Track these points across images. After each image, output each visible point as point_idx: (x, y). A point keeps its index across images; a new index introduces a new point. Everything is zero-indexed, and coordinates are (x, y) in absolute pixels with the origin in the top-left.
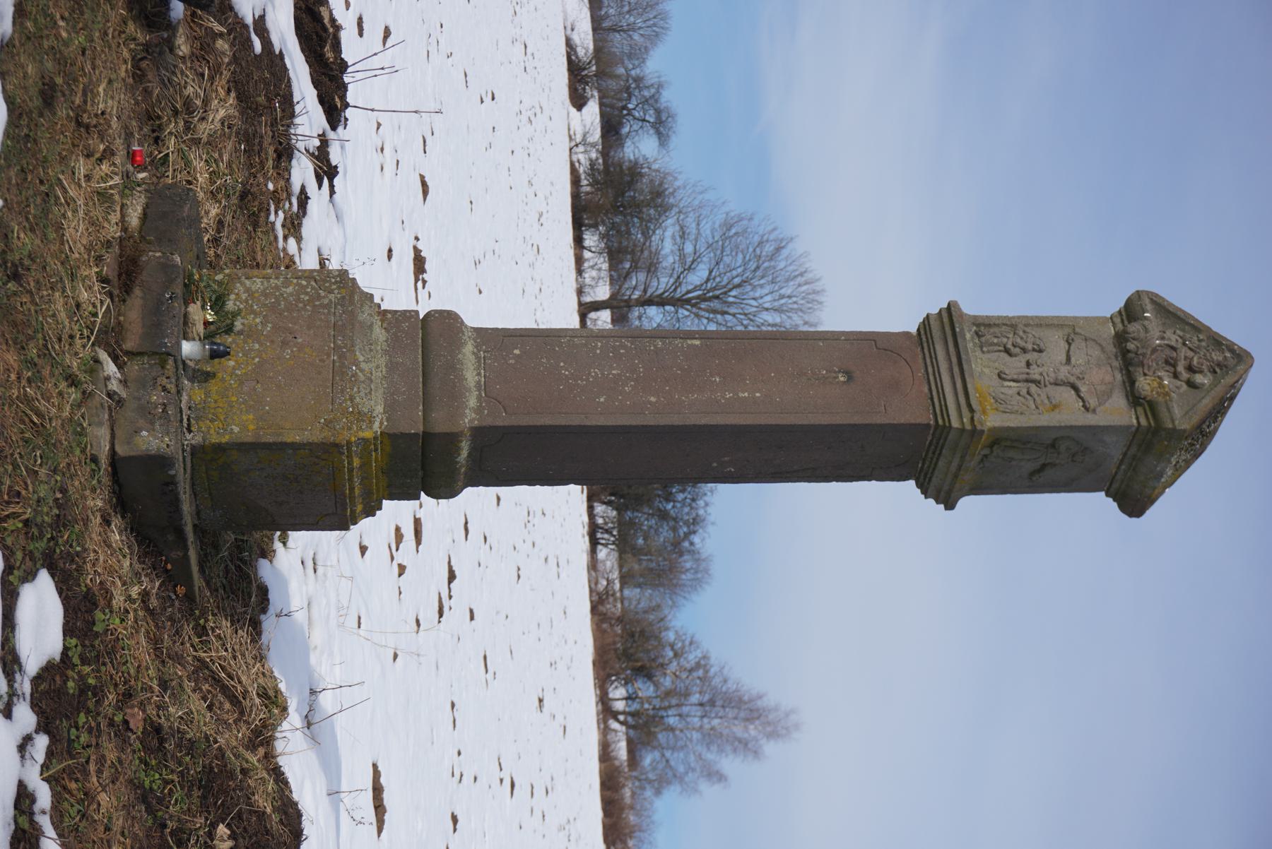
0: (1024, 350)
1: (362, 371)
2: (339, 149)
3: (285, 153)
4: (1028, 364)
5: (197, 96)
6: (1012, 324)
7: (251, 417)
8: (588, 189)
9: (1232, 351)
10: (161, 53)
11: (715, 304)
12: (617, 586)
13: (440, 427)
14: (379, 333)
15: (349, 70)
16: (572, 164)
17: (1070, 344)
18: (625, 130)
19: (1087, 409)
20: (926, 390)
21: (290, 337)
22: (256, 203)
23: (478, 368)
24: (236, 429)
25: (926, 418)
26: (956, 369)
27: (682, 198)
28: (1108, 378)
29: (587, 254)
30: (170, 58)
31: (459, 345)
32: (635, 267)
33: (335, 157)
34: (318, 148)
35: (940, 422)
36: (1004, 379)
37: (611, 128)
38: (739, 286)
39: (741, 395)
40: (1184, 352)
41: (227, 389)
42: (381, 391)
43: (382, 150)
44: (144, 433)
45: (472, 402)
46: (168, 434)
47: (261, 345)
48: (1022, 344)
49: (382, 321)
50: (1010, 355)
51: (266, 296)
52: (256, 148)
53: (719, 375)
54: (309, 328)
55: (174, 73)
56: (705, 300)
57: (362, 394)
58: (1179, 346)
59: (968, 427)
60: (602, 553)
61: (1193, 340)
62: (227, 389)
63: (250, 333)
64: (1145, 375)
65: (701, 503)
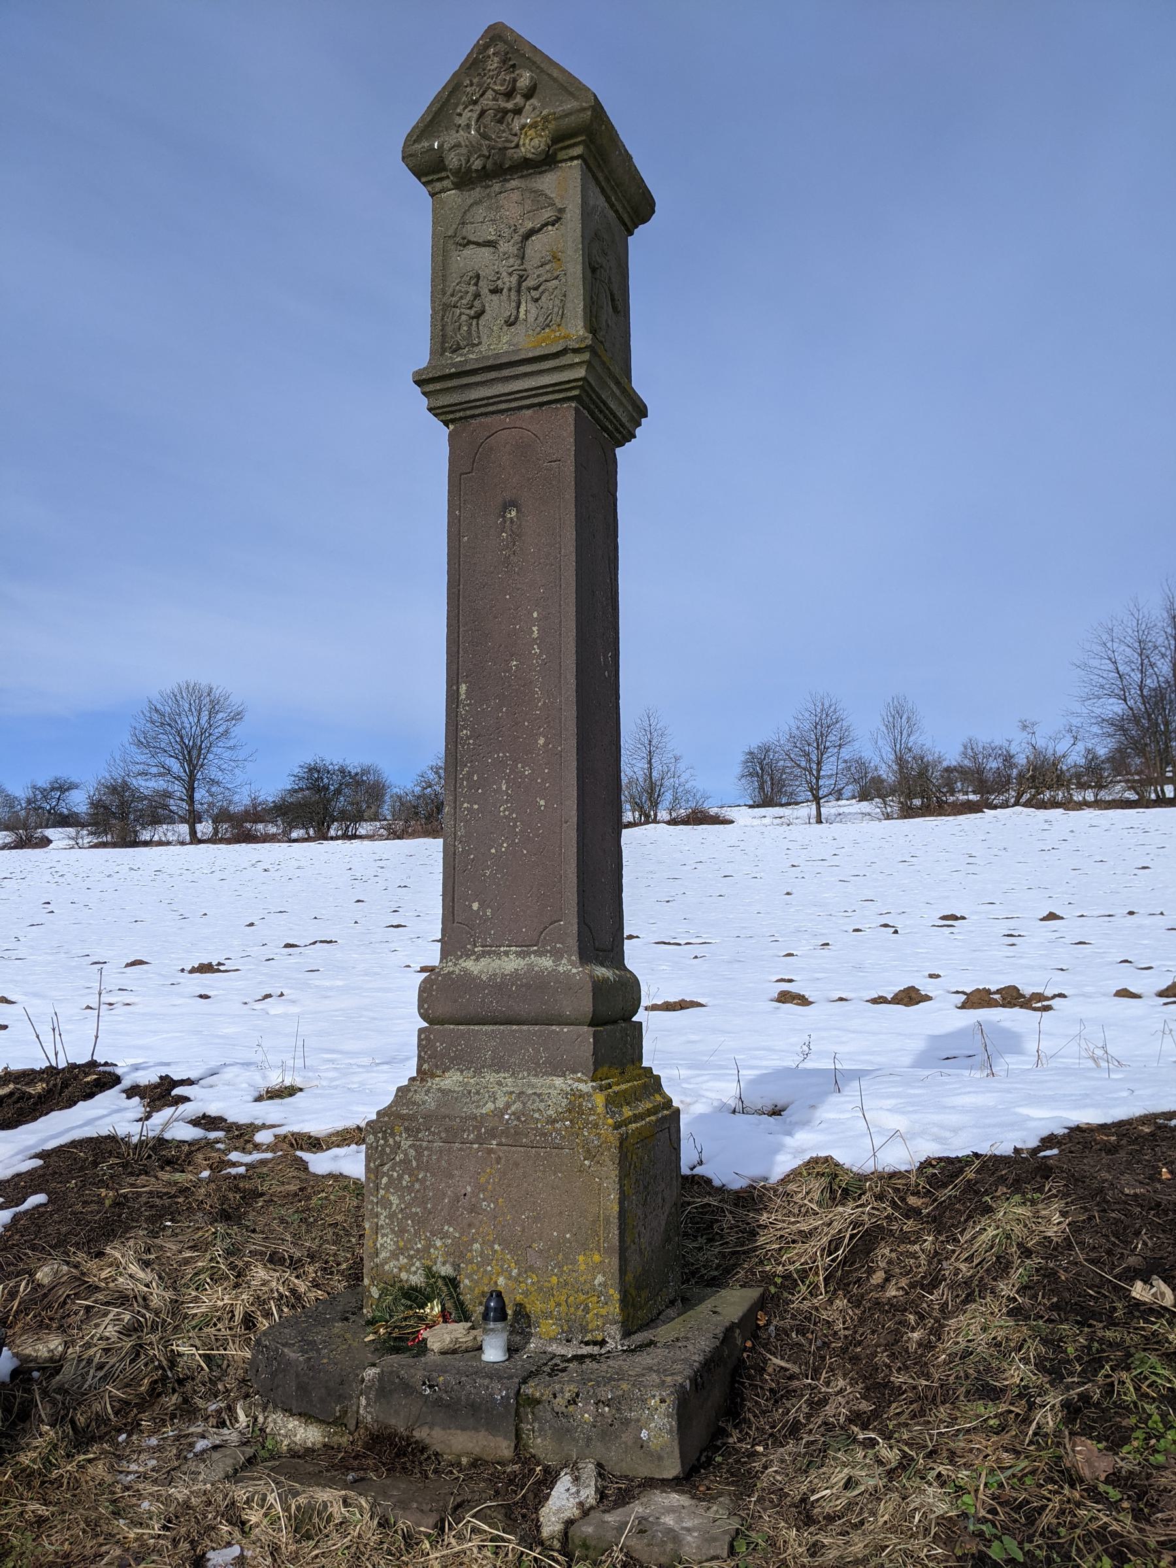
0: (477, 295)
1: (508, 1105)
2: (140, 1073)
3: (162, 1153)
4: (496, 291)
5: (117, 1319)
6: (442, 309)
7: (581, 1258)
8: (109, 837)
9: (486, 47)
10: (61, 1390)
11: (195, 753)
12: (385, 823)
13: (586, 1005)
14: (452, 1080)
15: (54, 1064)
16: (91, 847)
17: (470, 242)
18: (66, 812)
19: (558, 219)
20: (529, 412)
21: (464, 1201)
22: (231, 1195)
23: (498, 954)
24: (600, 1279)
25: (567, 414)
26: (506, 373)
27: (118, 774)
28: (516, 196)
29: (156, 838)
30: (68, 1372)
31: (467, 982)
32: (165, 807)
33: (147, 1077)
34: (142, 1098)
35: (576, 392)
36: (517, 318)
37: (64, 821)
38: (182, 738)
39: (535, 635)
40: (487, 101)
41: (540, 1289)
42: (534, 1080)
43: (111, 1004)
44: (644, 1434)
45: (546, 962)
46: (644, 1401)
47: (474, 1240)
48: (469, 297)
49: (433, 1076)
50: (483, 312)
51: (403, 1231)
52: (167, 1201)
53: (507, 662)
54: (451, 1176)
55: (90, 1361)
56: (191, 760)
57: (542, 1106)
58: (478, 108)
59: (586, 356)
60: (362, 831)
61: (473, 91)
62: (540, 1289)
63: (458, 1254)
64: (517, 146)
65: (330, 767)
